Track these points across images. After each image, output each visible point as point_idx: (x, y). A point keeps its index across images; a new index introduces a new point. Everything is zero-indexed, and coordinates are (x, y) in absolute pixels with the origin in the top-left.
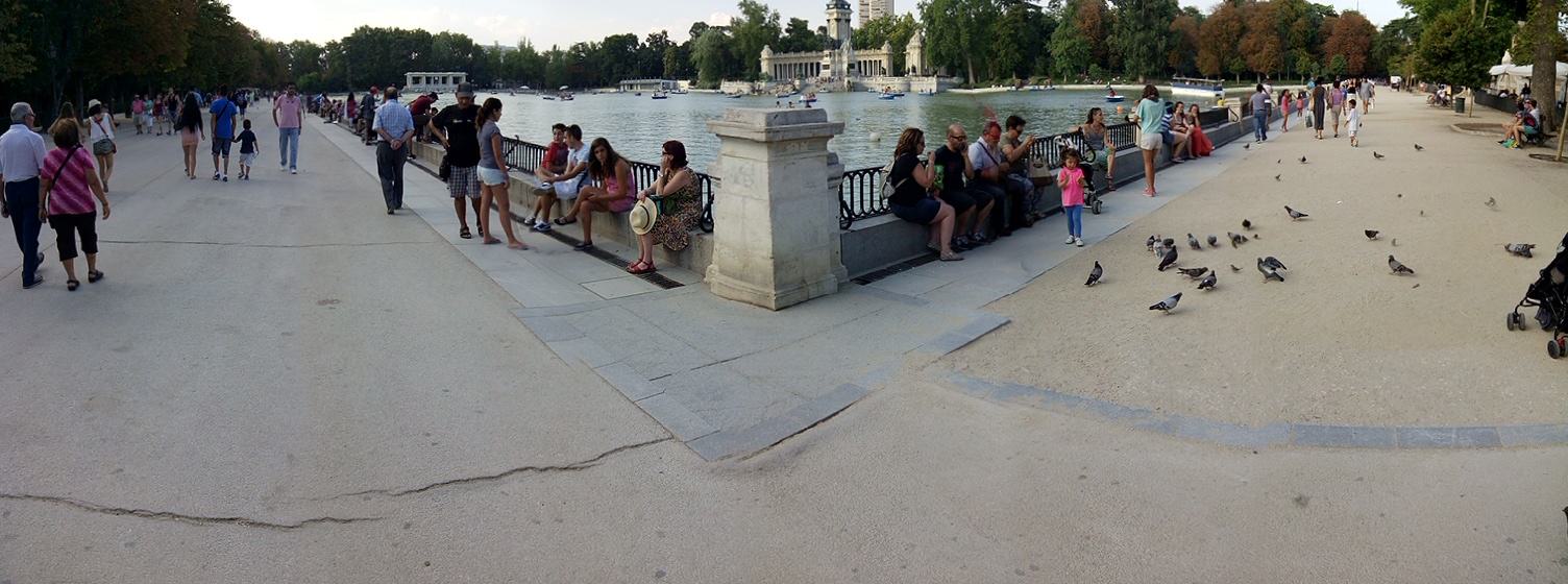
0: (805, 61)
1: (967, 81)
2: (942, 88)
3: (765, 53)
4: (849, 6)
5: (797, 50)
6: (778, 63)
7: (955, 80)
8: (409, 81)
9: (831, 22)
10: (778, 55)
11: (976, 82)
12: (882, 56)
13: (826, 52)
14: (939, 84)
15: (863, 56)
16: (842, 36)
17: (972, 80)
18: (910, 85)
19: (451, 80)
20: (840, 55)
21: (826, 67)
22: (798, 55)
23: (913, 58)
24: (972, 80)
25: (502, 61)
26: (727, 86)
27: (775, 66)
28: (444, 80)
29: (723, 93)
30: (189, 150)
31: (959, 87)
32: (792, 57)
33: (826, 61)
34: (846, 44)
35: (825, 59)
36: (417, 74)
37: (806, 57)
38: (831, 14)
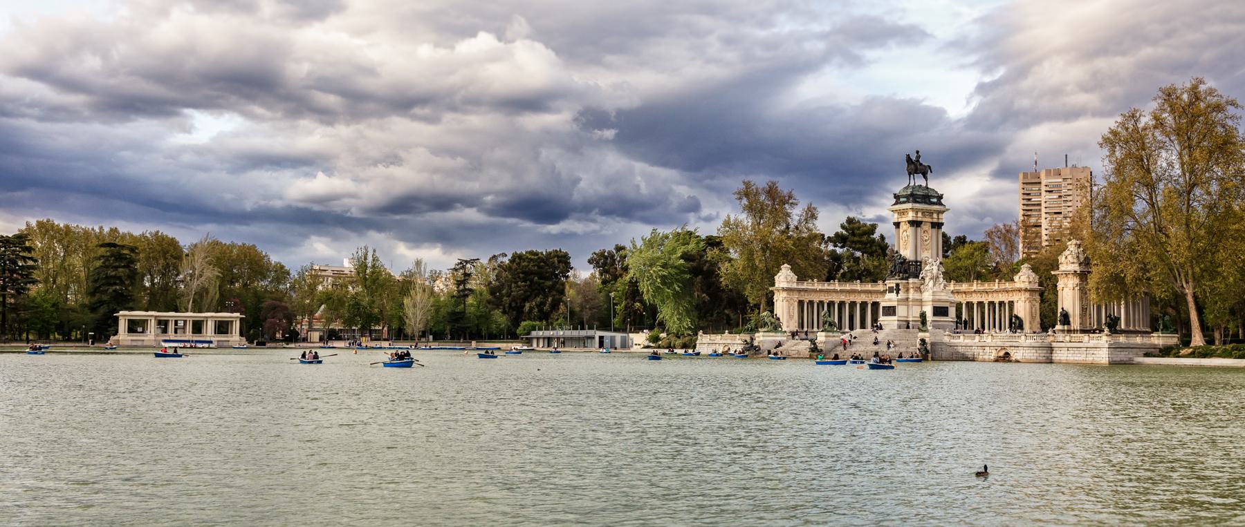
0: (863, 298)
1: (1186, 342)
2: (1122, 356)
3: (784, 277)
4: (940, 197)
5: (849, 277)
6: (806, 298)
7: (1158, 339)
8: (123, 325)
9: (903, 226)
10: (805, 286)
11: (1210, 341)
12: (1018, 294)
13: (891, 283)
14: (1113, 347)
15: (975, 292)
16: (924, 255)
17: (1198, 340)
18: (1051, 349)
19: (210, 327)
20: (918, 290)
21: (890, 311)
22: (848, 287)
23: (1068, 297)
24: (1198, 340)
25: (643, 186)
26: (707, 343)
27: (801, 303)
28: (198, 327)
29: (698, 354)
30: (375, 259)
31: (1166, 351)
32: (837, 291)
33: (889, 299)
34: (932, 268)
35: (888, 296)
36: (138, 314)
37: (858, 292)
38: (902, 213)
